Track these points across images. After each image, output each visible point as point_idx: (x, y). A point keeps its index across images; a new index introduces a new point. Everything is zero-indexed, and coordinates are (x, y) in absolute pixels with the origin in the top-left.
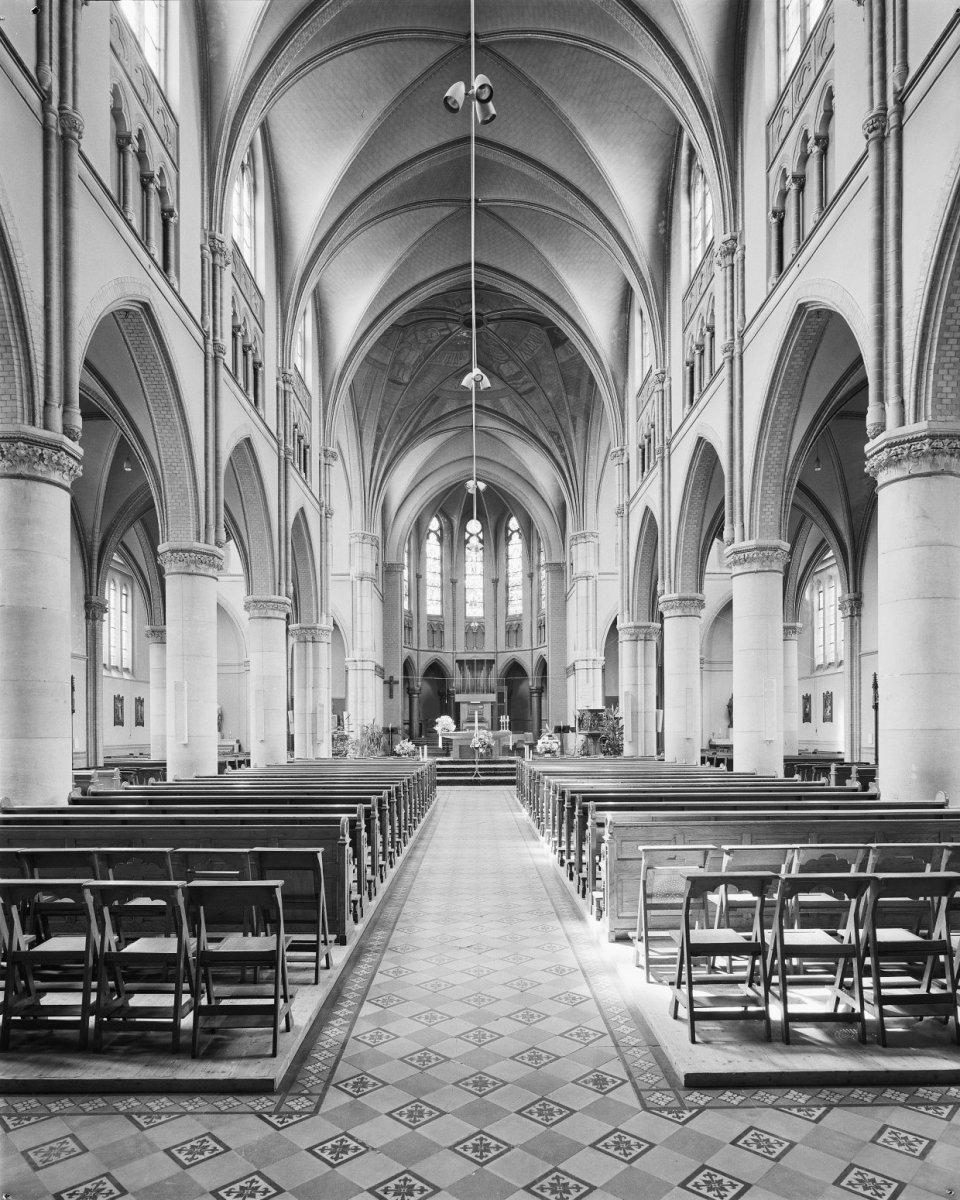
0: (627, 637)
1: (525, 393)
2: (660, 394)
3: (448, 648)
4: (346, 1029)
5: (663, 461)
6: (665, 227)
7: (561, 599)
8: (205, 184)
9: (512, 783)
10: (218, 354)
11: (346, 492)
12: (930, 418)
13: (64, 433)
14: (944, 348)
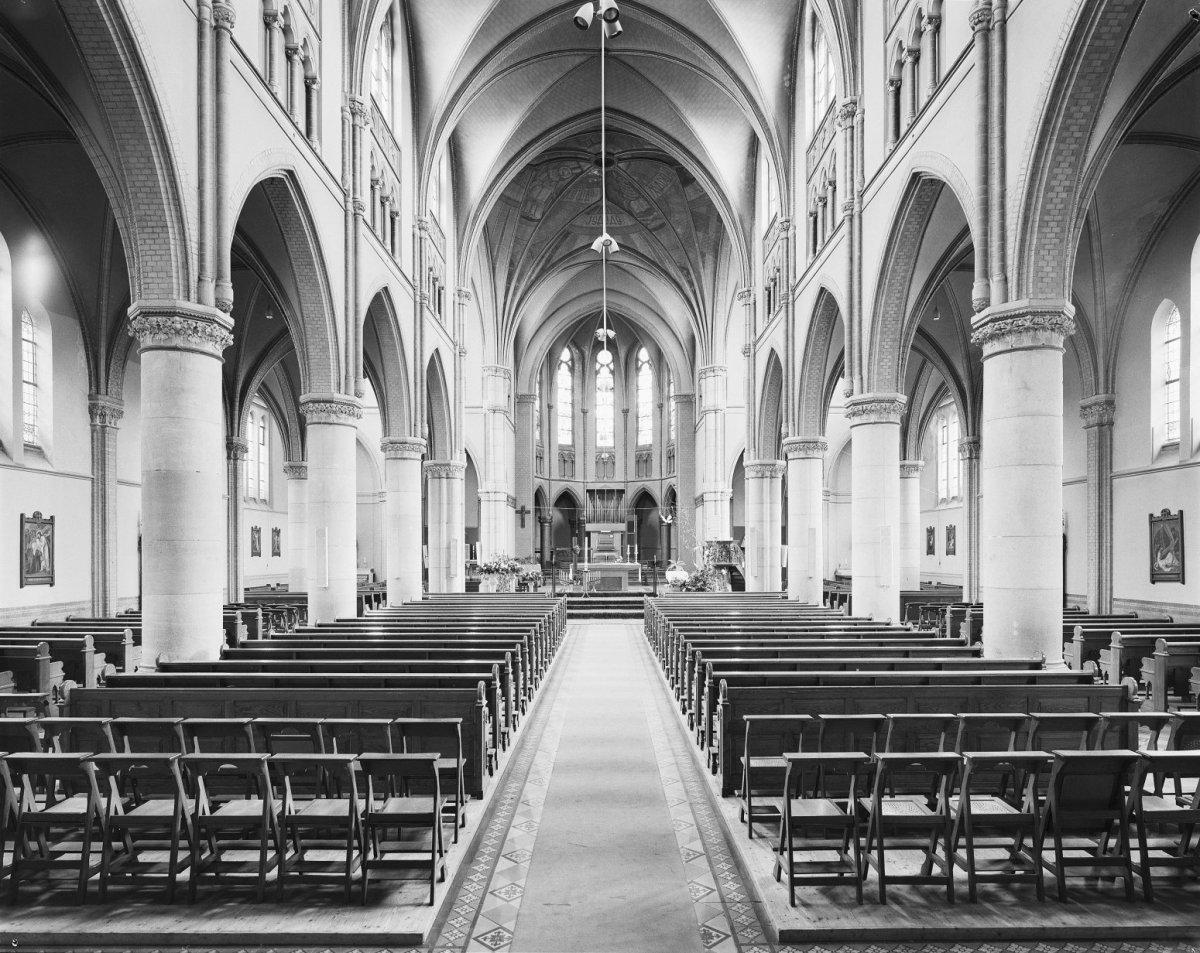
0: (753, 474)
1: (655, 229)
2: (785, 240)
3: (579, 477)
4: (484, 884)
5: (787, 307)
6: (790, 80)
7: (690, 430)
8: (346, 49)
9: (640, 616)
10: (358, 211)
11: (479, 324)
12: (1031, 296)
13: (217, 306)
14: (1044, 230)
